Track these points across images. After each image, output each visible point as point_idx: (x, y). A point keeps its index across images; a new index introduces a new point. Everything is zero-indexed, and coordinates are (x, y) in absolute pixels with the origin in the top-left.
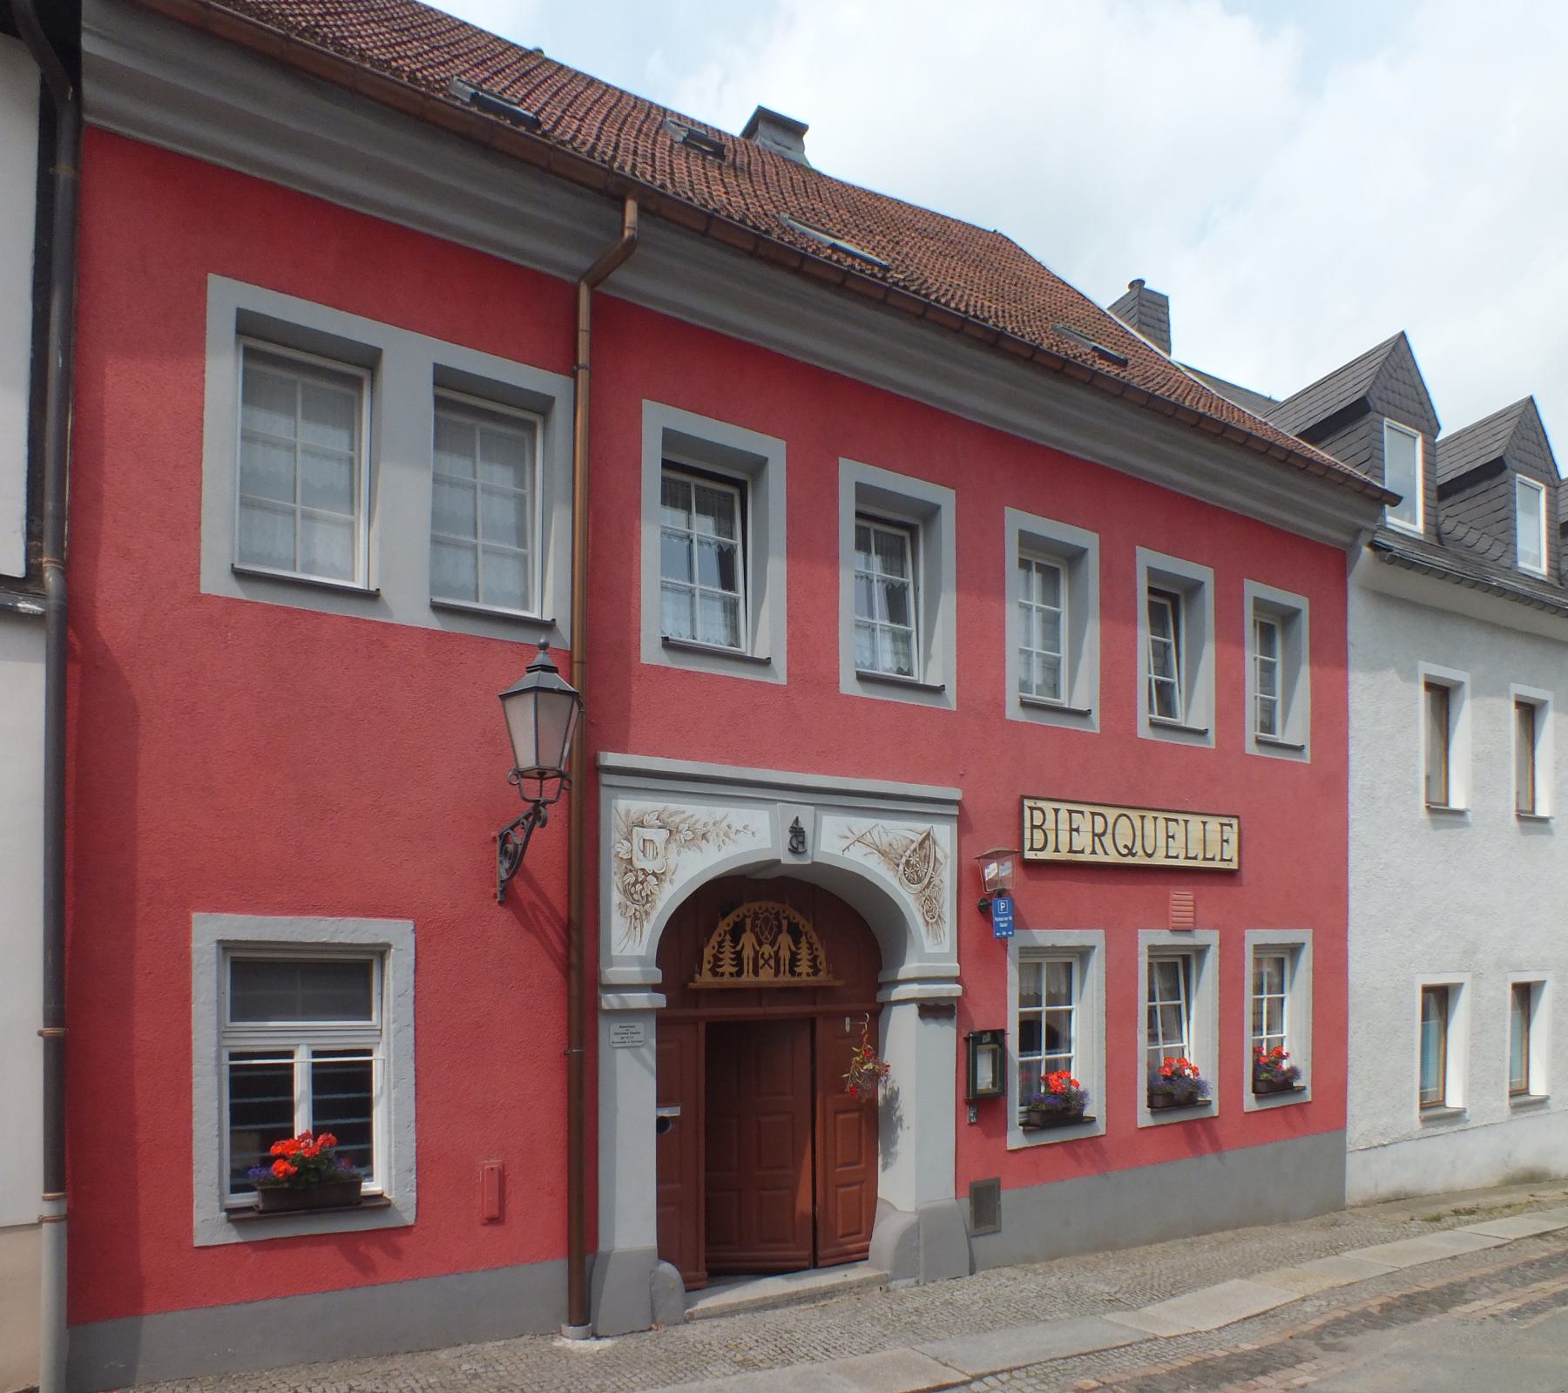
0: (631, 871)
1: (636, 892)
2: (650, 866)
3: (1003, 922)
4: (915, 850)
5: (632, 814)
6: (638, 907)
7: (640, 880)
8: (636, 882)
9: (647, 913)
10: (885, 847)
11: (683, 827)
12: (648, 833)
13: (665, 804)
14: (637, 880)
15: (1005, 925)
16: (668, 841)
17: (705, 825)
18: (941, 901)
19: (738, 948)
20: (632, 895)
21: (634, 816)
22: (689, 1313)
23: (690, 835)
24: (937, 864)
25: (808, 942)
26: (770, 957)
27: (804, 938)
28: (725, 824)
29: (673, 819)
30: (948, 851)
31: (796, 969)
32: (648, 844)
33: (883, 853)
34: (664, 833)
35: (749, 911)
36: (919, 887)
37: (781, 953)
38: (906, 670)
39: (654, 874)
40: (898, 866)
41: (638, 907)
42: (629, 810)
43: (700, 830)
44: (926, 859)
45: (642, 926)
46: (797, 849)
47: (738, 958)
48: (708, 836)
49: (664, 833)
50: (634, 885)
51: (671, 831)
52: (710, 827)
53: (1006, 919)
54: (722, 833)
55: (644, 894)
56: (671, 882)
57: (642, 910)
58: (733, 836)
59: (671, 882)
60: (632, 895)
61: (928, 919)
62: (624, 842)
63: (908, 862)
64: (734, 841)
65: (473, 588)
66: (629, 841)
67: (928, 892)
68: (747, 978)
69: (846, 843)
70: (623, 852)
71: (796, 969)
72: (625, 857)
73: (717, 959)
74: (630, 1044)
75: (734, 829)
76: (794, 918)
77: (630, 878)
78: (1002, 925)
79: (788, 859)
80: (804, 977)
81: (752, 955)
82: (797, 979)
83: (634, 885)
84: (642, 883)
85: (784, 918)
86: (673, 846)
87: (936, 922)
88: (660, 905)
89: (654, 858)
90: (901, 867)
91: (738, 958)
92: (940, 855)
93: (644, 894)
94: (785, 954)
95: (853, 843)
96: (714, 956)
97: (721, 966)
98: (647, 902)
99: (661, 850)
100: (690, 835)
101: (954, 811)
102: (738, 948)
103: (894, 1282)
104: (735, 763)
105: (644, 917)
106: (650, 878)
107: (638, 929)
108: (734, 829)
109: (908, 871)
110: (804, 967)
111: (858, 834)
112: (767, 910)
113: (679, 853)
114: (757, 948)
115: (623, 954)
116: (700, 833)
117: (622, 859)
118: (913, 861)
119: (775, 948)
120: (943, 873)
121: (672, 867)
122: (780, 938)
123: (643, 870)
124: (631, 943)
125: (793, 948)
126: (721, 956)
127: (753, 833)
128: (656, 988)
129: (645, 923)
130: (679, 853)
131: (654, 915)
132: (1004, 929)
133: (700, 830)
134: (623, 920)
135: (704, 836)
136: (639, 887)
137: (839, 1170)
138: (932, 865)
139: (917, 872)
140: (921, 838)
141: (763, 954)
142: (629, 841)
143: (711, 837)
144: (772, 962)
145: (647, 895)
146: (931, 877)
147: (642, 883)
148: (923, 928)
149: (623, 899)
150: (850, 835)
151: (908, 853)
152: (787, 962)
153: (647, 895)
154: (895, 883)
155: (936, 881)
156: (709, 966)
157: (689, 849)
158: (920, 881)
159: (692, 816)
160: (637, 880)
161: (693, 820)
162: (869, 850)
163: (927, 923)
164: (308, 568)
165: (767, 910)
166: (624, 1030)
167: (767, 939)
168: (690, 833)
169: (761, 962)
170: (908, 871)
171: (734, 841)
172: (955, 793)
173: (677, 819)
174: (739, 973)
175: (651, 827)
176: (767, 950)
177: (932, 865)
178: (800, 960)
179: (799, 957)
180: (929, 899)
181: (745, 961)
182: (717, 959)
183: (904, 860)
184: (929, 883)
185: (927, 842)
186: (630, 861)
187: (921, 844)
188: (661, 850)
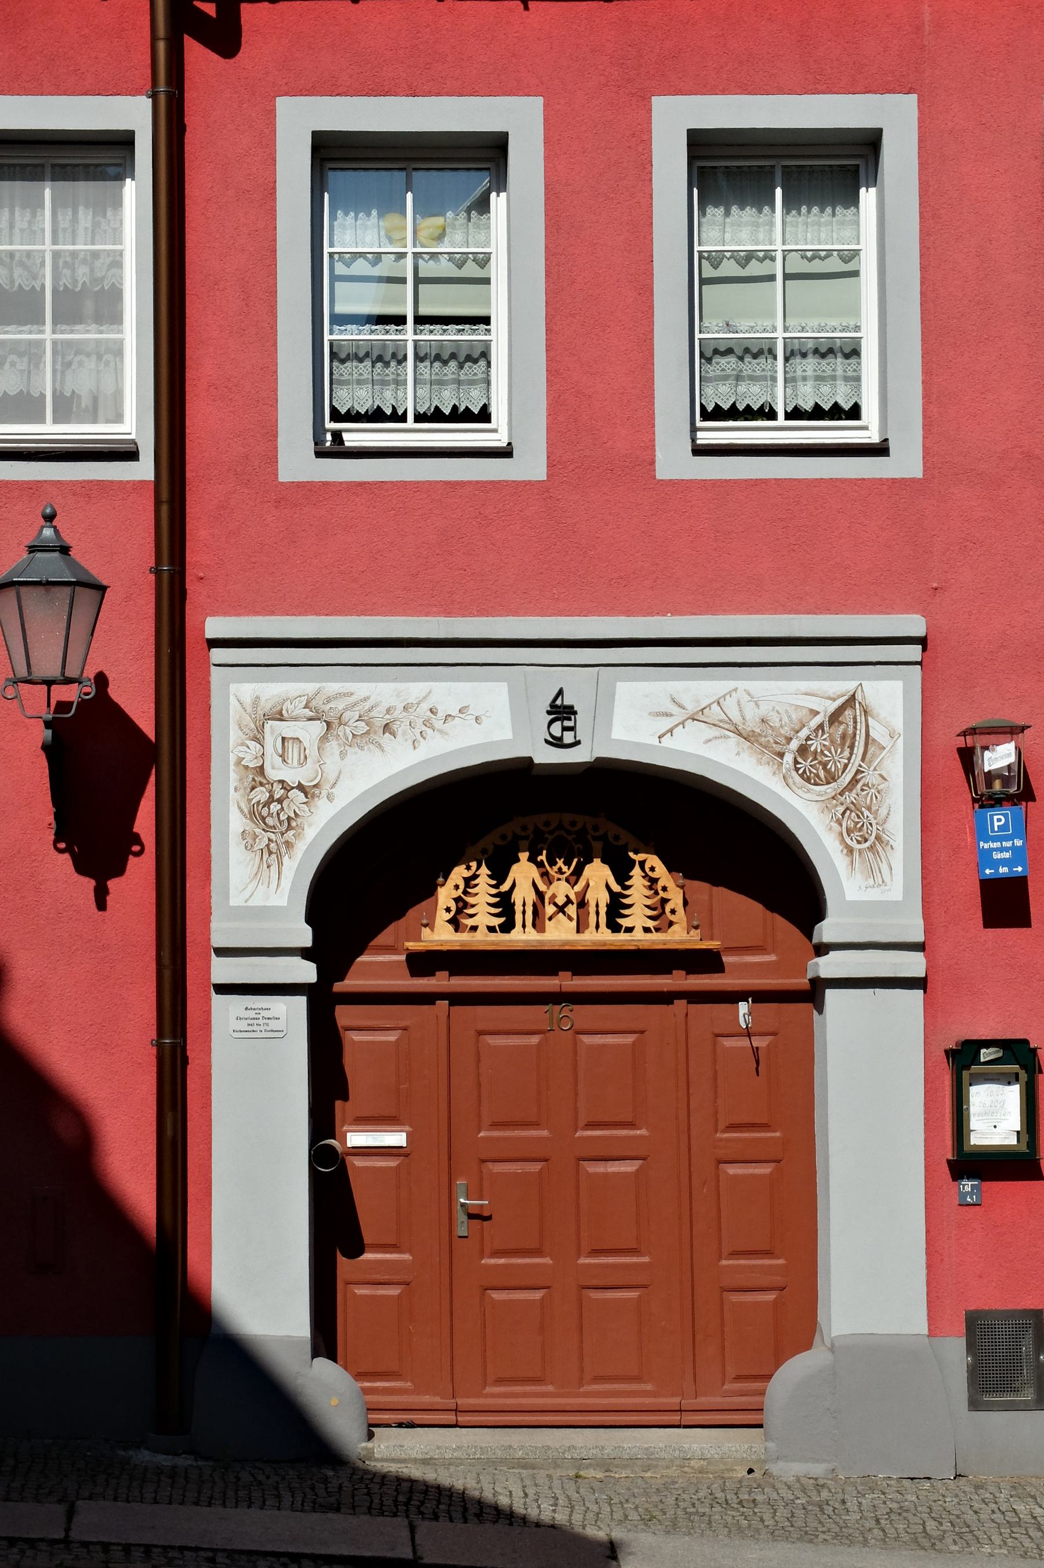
0: (261, 784)
1: (270, 815)
2: (292, 777)
3: (1002, 850)
4: (821, 726)
5: (262, 702)
6: (273, 836)
7: (276, 796)
8: (271, 799)
9: (288, 844)
10: (752, 724)
11: (351, 716)
12: (287, 729)
13: (317, 685)
14: (271, 797)
15: (1007, 855)
16: (324, 739)
17: (388, 711)
18: (883, 812)
19: (505, 887)
20: (263, 819)
21: (266, 706)
22: (366, 1448)
23: (363, 728)
24: (872, 749)
25: (646, 876)
26: (569, 901)
27: (636, 871)
28: (425, 706)
29: (332, 705)
30: (898, 724)
31: (620, 921)
32: (289, 745)
33: (749, 738)
34: (319, 727)
35: (524, 828)
36: (830, 789)
37: (590, 896)
38: (847, 407)
39: (301, 787)
40: (781, 755)
41: (273, 836)
42: (258, 697)
43: (379, 718)
44: (848, 741)
45: (280, 864)
46: (561, 739)
47: (505, 904)
48: (395, 727)
49: (319, 727)
50: (267, 804)
51: (328, 724)
52: (398, 713)
53: (1009, 844)
54: (420, 722)
55: (283, 817)
56: (330, 798)
57: (280, 840)
58: (438, 724)
59: (330, 798)
60: (263, 819)
61: (854, 844)
62: (252, 744)
63: (803, 750)
64: (441, 731)
65: (383, 286)
66: (259, 740)
67: (850, 797)
68: (523, 937)
69: (666, 724)
70: (248, 757)
71: (620, 921)
72: (251, 765)
73: (462, 905)
74: (264, 1035)
75: (441, 714)
76: (617, 838)
77: (261, 794)
78: (997, 856)
79: (547, 756)
80: (638, 935)
81: (531, 897)
82: (622, 936)
83: (267, 804)
84: (280, 801)
85: (596, 839)
86: (333, 746)
87: (871, 848)
88: (310, 833)
89: (301, 765)
90: (789, 758)
91: (505, 904)
92: (877, 732)
93: (283, 817)
94: (599, 897)
95: (683, 723)
96: (457, 900)
97: (472, 916)
98: (289, 828)
99: (312, 752)
100: (363, 728)
101: (914, 652)
102: (505, 887)
103: (781, 1464)
104: (448, 613)
105: (283, 850)
106: (295, 794)
107: (274, 868)
108: (441, 714)
109: (803, 764)
110: (637, 917)
111: (691, 707)
112: (560, 826)
113: (343, 755)
114: (542, 887)
115: (250, 903)
116: (379, 723)
117: (246, 767)
118: (815, 745)
119: (578, 888)
120: (886, 763)
121: (332, 777)
122: (589, 870)
123: (282, 782)
124: (262, 888)
125: (616, 888)
126: (470, 900)
127: (477, 719)
128: (306, 954)
129: (286, 859)
130: (343, 755)
131: (301, 848)
132: (1003, 862)
133: (379, 718)
134: (249, 855)
135: (387, 728)
136: (275, 807)
137: (724, 1262)
138: (859, 750)
139: (825, 765)
140: (833, 706)
141: (554, 896)
142: (259, 740)
143: (400, 728)
144: (572, 910)
145: (289, 819)
146: (858, 772)
147: (280, 801)
148: (840, 861)
149: (250, 826)
150: (675, 710)
151: (804, 733)
152: (603, 910)
153: (289, 819)
154: (776, 785)
155: (870, 777)
156: (449, 916)
157: (362, 748)
158: (831, 778)
159: (366, 699)
160: (271, 797)
161: (367, 705)
162: (715, 732)
163: (850, 851)
164: (333, 217)
165: (560, 826)
166: (252, 1014)
167: (560, 871)
168: (362, 724)
169: (550, 909)
170: (803, 764)
171: (441, 731)
172: (915, 625)
173: (340, 705)
174: (507, 927)
175: (296, 719)
176: (561, 890)
177: (859, 750)
178: (629, 906)
179: (625, 901)
180: (854, 808)
181: (518, 908)
182: (462, 905)
183: (794, 745)
184: (854, 781)
185: (848, 713)
186: (261, 770)
187: (835, 717)
188: (312, 752)
